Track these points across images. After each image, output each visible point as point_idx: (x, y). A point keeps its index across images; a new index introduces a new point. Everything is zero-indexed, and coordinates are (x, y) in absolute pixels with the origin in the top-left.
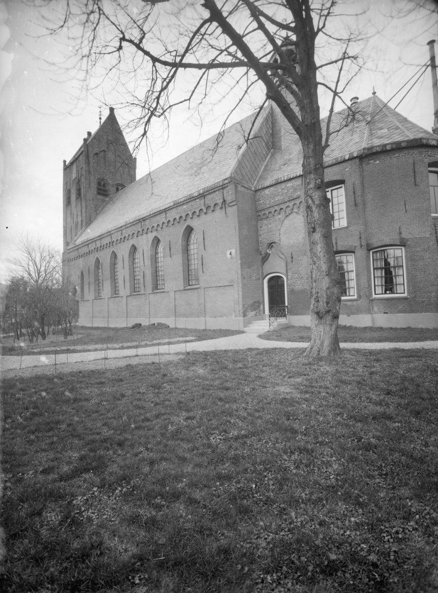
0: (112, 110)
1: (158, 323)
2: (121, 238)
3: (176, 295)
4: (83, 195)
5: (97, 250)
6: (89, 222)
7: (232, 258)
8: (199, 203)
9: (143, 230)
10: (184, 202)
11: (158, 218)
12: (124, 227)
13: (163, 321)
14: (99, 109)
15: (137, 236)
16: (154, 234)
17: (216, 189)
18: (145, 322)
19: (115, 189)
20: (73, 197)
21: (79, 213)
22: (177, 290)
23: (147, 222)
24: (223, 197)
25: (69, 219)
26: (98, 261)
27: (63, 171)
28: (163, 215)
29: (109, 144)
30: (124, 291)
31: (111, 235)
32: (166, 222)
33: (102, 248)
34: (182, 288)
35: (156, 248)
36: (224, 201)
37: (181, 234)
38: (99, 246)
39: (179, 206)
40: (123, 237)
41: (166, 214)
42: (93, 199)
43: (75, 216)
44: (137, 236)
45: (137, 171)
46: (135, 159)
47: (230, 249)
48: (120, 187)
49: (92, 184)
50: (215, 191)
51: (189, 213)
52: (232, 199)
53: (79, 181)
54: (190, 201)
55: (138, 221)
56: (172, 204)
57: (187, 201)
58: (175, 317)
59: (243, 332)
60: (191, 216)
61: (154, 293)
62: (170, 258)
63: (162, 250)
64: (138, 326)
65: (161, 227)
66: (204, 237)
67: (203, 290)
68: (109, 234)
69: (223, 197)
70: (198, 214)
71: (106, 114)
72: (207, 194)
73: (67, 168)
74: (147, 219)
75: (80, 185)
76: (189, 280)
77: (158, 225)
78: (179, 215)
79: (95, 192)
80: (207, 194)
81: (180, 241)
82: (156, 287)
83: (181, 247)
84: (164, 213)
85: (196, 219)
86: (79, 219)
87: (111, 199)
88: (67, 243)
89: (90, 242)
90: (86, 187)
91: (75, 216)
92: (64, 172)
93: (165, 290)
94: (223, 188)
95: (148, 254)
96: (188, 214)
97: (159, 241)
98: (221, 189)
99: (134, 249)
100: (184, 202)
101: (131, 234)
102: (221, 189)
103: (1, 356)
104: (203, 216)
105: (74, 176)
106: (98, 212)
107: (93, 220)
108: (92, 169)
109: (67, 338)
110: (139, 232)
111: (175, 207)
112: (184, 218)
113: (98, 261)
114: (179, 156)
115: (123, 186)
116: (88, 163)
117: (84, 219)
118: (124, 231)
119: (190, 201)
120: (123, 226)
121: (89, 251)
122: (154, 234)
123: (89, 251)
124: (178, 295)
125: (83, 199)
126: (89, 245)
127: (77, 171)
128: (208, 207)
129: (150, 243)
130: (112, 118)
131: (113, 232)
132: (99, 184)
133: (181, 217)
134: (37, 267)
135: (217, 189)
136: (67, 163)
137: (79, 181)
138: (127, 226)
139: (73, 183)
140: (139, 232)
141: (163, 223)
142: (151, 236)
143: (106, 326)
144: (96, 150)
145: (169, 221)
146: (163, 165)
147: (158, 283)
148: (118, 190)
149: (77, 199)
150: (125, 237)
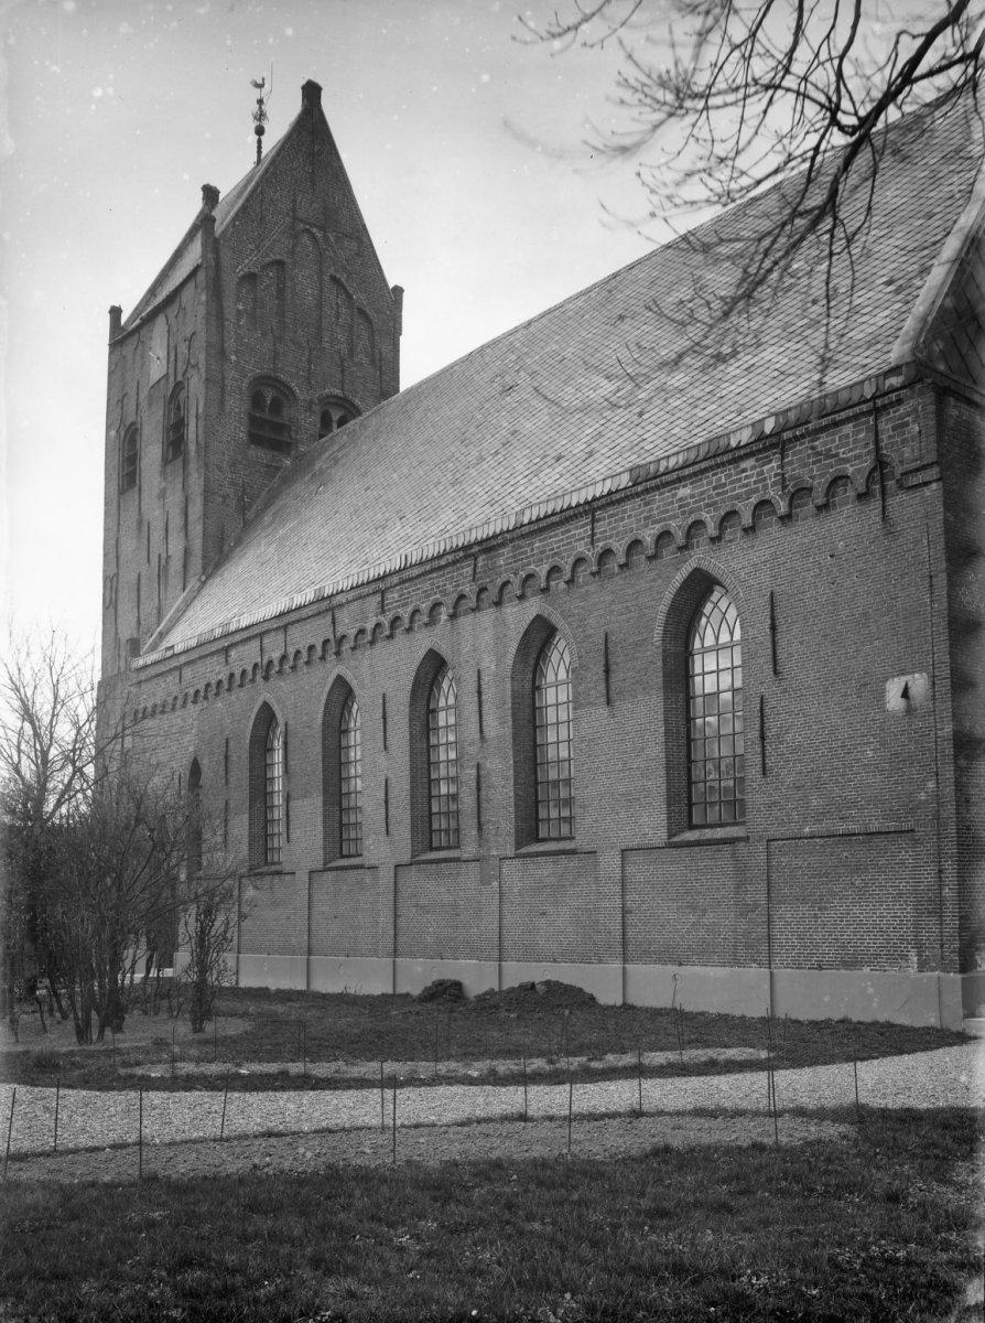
0: (312, 92)
1: (548, 983)
2: (378, 625)
3: (630, 869)
4: (192, 448)
5: (266, 671)
6: (217, 553)
7: (910, 710)
8: (758, 478)
9: (483, 590)
10: (686, 472)
11: (555, 540)
12: (395, 579)
13: (568, 974)
14: (256, 94)
15: (453, 617)
16: (533, 607)
17: (843, 415)
18: (478, 978)
19: (315, 419)
20: (152, 453)
21: (176, 522)
22: (635, 843)
23: (503, 557)
24: (878, 448)
25: (129, 545)
26: (267, 717)
27: (106, 349)
28: (580, 530)
29: (296, 237)
30: (383, 845)
31: (332, 609)
32: (591, 555)
33: (289, 663)
34: (661, 836)
35: (537, 664)
36: (881, 464)
37: (663, 608)
38: (276, 655)
39: (657, 488)
40: (386, 620)
41: (593, 521)
42: (233, 464)
43: (157, 536)
44: (453, 617)
45: (406, 343)
46: (398, 291)
47: (903, 673)
48: (339, 412)
49: (230, 402)
50: (836, 424)
51: (705, 516)
52: (921, 458)
53: (179, 386)
54: (711, 468)
55: (461, 554)
56: (625, 480)
57: (697, 468)
58: (625, 961)
59: (963, 1038)
60: (712, 530)
61: (525, 856)
62: (603, 711)
63: (562, 675)
64: (447, 993)
65: (568, 576)
66: (773, 618)
67: (762, 847)
68: (324, 605)
69: (878, 448)
70: (747, 520)
71: (283, 116)
72: (796, 438)
73: (125, 338)
74: (503, 545)
75: (178, 408)
76: (690, 805)
77: (554, 570)
78: (657, 529)
79: (243, 436)
80: (796, 438)
81: (658, 632)
82: (529, 830)
83: (660, 664)
84: (586, 520)
85: (736, 546)
86: (176, 547)
87: (303, 465)
88: (122, 645)
89: (238, 638)
90: (207, 416)
91: (157, 536)
92: (111, 353)
93: (580, 842)
94: (877, 412)
95: (499, 693)
96: (699, 524)
97: (551, 631)
98: (869, 413)
99: (434, 668)
100: (686, 472)
101: (425, 606)
102: (869, 413)
103: (977, 1103)
104: (773, 532)
105: (157, 368)
106: (250, 515)
107: (232, 550)
108: (230, 344)
109: (201, 1030)
110: (462, 597)
111: (638, 495)
112: (680, 538)
113: (267, 717)
114: (615, 275)
115: (350, 411)
116: (217, 315)
117: (197, 544)
118: (393, 596)
119: (711, 468)
120: (391, 574)
121: (232, 675)
122: (533, 607)
123: (232, 675)
124: (639, 870)
125: (193, 466)
126: (233, 653)
127: (172, 350)
128: (799, 494)
129: (513, 647)
130: (312, 130)
131: (341, 599)
132: (257, 400)
133: (665, 535)
134: (41, 744)
135: (850, 412)
136: (124, 318)
137: (179, 386)
138: (405, 575)
139: (150, 397)
140: (462, 597)
141: (580, 561)
142: (518, 616)
143: (301, 986)
144: (248, 264)
145: (607, 553)
146: (542, 316)
147: (542, 814)
148: (326, 423)
149: (166, 461)
150: (397, 618)
